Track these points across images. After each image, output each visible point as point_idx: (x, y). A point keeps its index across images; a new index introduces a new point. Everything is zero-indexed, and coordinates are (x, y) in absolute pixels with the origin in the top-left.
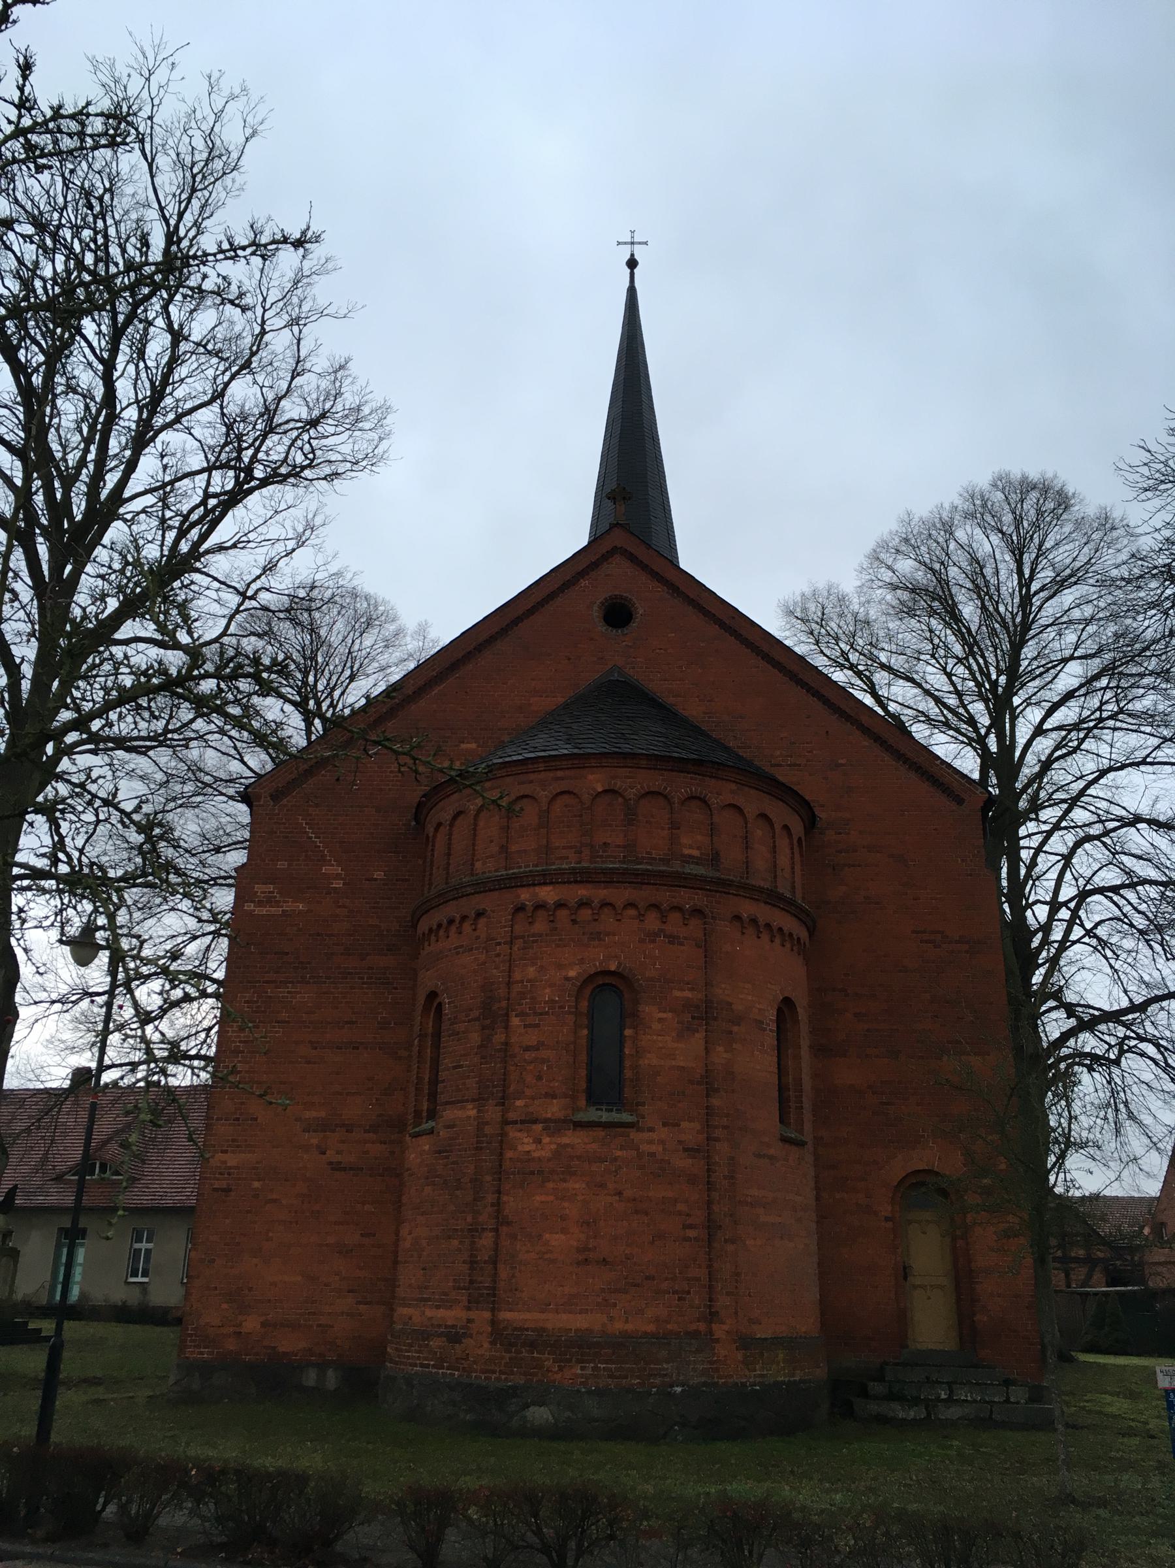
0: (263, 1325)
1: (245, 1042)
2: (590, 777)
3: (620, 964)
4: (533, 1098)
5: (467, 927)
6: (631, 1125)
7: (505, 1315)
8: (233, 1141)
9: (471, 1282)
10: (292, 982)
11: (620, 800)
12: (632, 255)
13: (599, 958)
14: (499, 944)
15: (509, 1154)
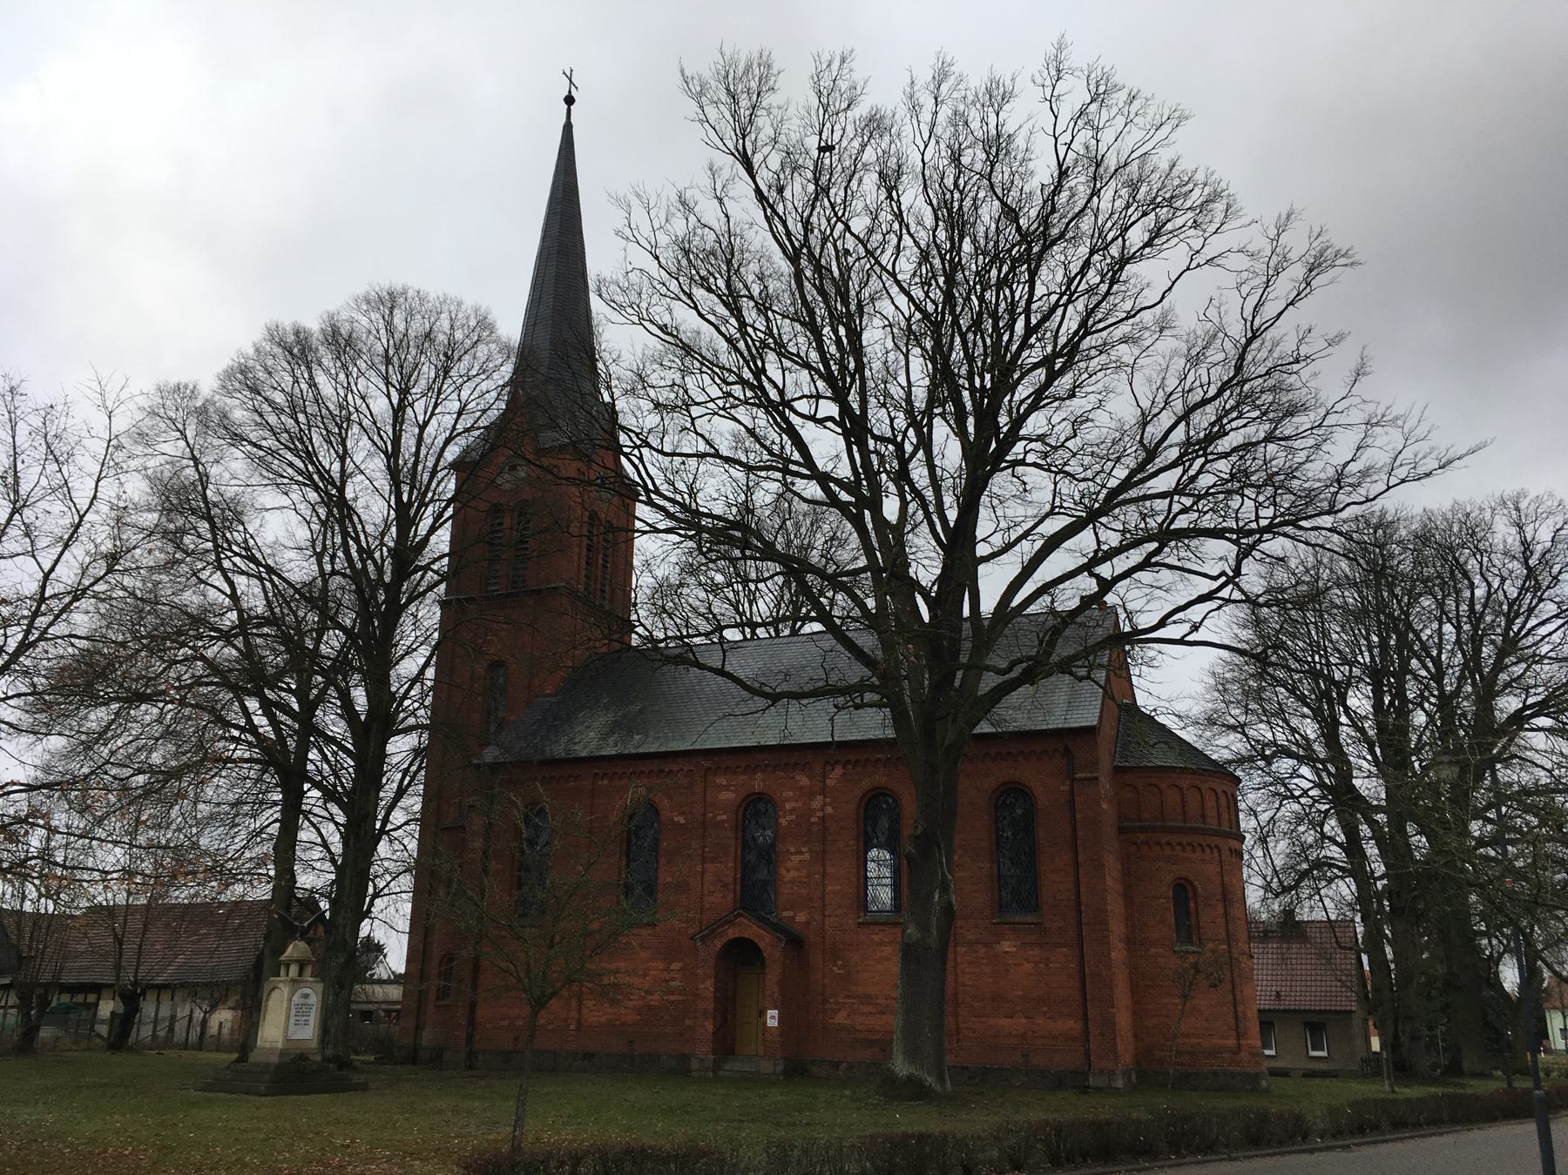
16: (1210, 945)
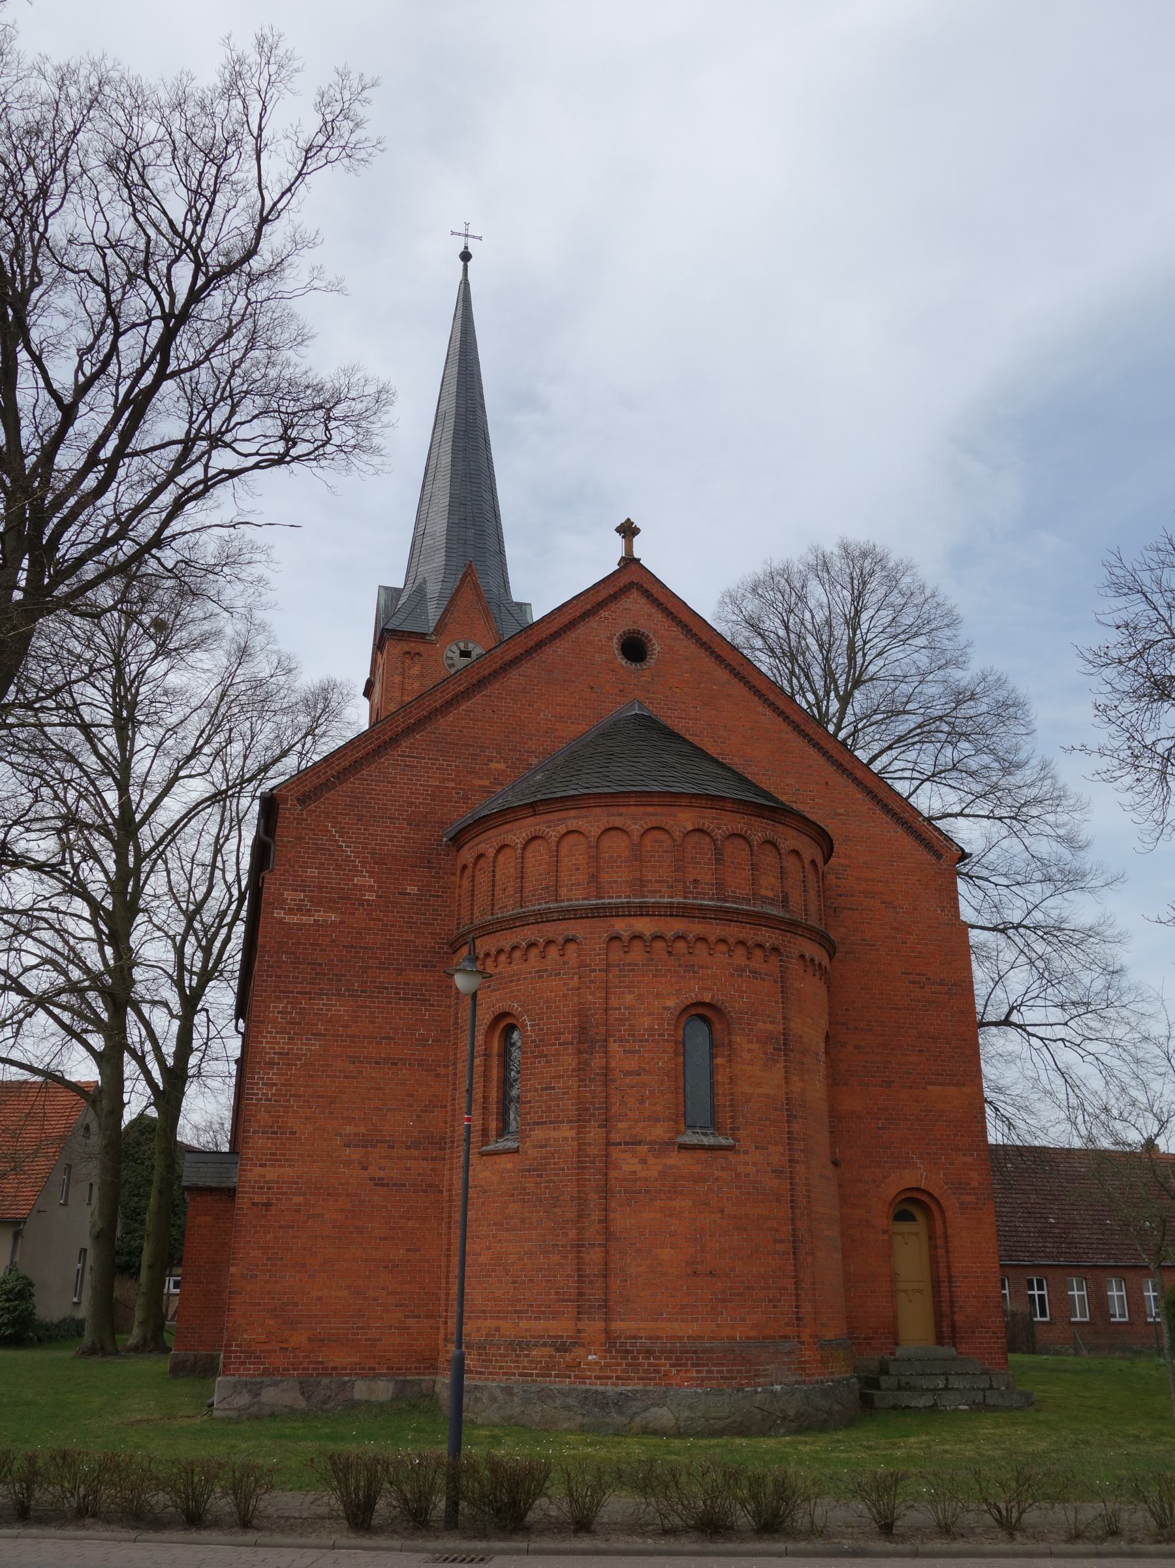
0: (309, 1339)
1: (280, 1054)
2: (680, 815)
3: (713, 997)
4: (637, 1121)
5: (553, 952)
6: (729, 1148)
7: (617, 1326)
8: (271, 1154)
9: (580, 1294)
10: (327, 994)
11: (707, 839)
12: (466, 248)
13: (695, 991)
14: (594, 970)
15: (613, 1174)
16: (539, 1134)
